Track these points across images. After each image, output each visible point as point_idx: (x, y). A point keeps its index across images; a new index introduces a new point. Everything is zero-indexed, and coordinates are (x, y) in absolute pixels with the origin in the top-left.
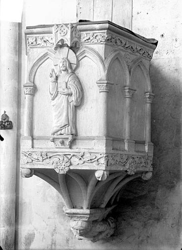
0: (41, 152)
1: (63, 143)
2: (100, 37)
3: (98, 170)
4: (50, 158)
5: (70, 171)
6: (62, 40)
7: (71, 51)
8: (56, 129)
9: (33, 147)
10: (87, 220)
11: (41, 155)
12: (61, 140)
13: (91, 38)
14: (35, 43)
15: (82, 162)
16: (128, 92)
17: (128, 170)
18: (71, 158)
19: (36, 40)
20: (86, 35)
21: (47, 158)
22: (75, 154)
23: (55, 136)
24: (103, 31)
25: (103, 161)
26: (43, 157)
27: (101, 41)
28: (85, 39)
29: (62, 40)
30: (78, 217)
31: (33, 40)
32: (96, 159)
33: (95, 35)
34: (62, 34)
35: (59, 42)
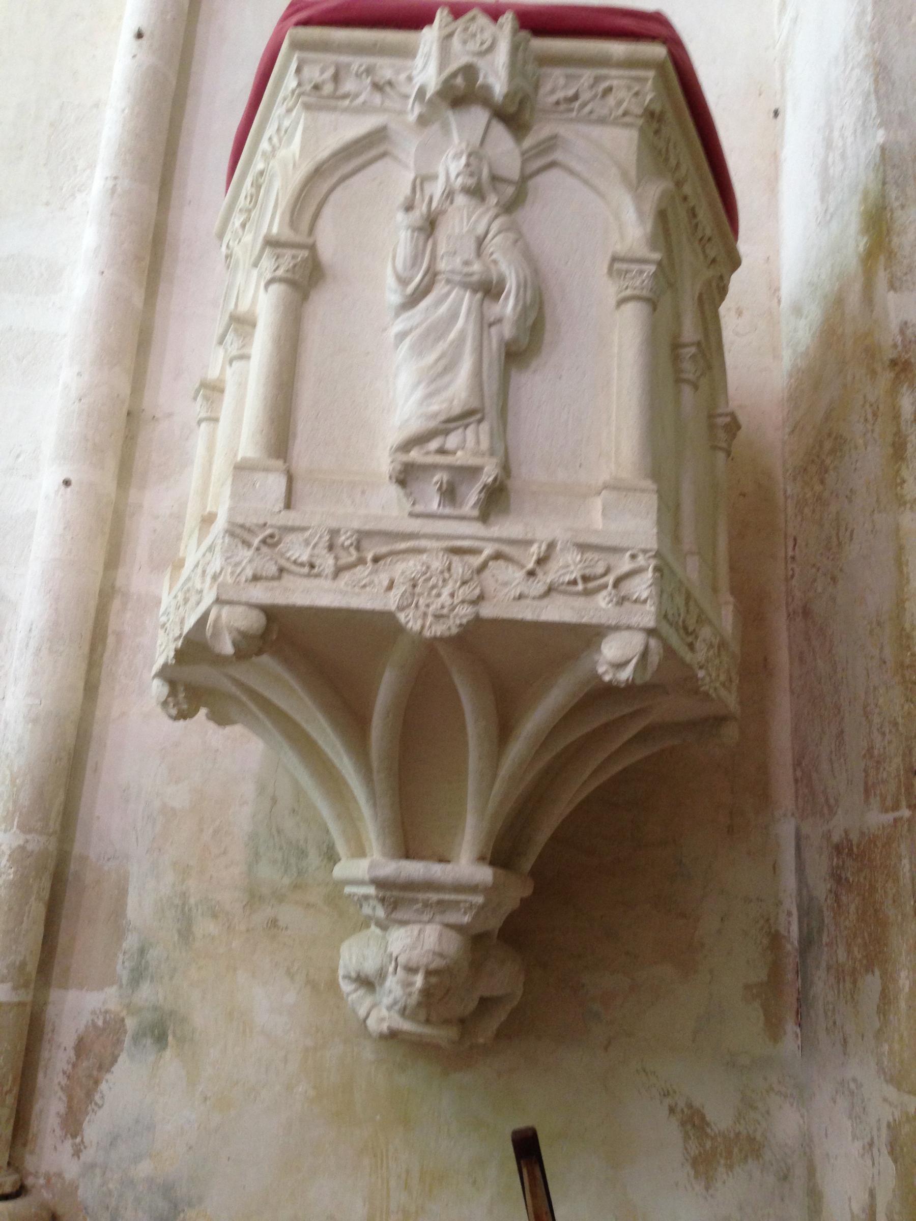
0: (334, 533)
1: (449, 494)
2: (622, 94)
3: (617, 628)
4: (376, 560)
5: (478, 621)
6: (469, 71)
7: (499, 131)
8: (416, 426)
9: (288, 505)
10: (466, 919)
11: (331, 547)
12: (440, 477)
13: (585, 96)
14: (328, 88)
15: (537, 587)
16: (693, 357)
17: (178, 918)
18: (484, 566)
19: (336, 78)
20: (562, 81)
21: (361, 561)
22: (506, 549)
23: (415, 455)
24: (641, 73)
25: (642, 586)
26: (336, 558)
27: (625, 114)
28: (560, 95)
29: (469, 71)
30: (426, 905)
31: (322, 72)
32: (610, 579)
33: (605, 84)
34: (473, 46)
35: (454, 75)
